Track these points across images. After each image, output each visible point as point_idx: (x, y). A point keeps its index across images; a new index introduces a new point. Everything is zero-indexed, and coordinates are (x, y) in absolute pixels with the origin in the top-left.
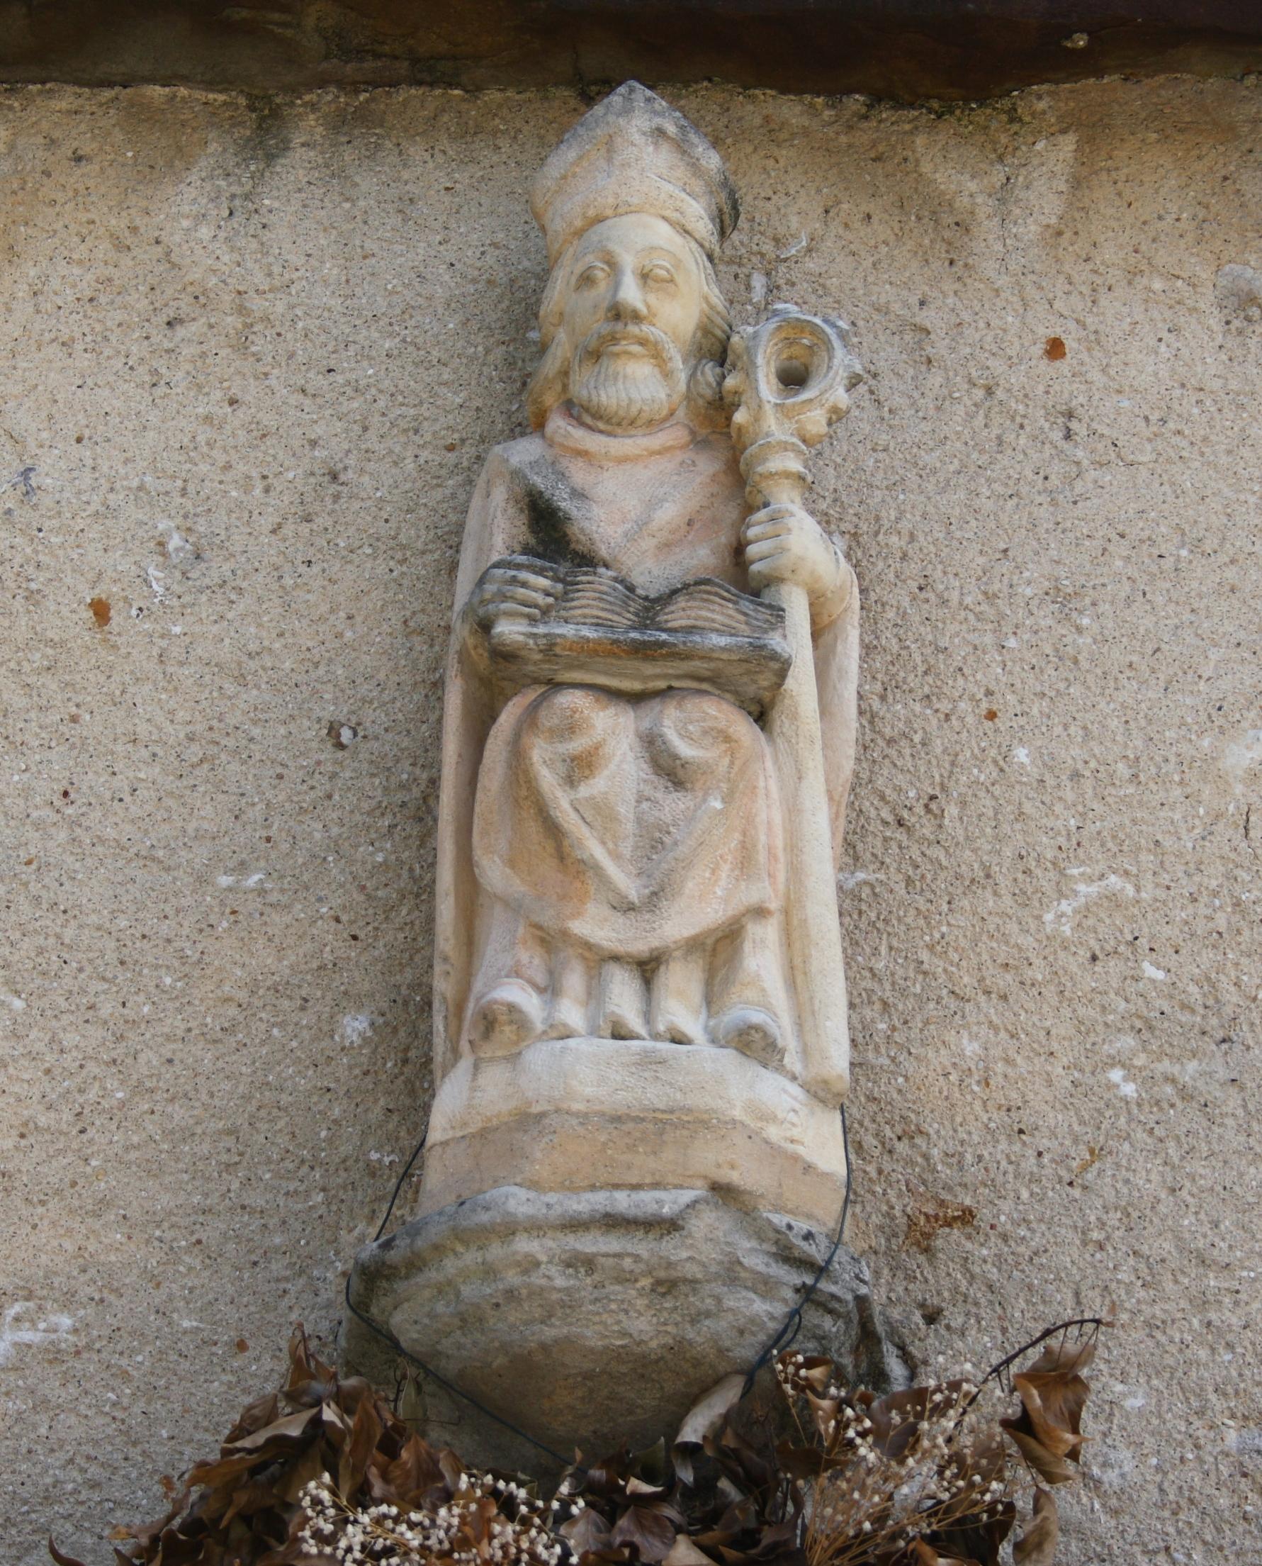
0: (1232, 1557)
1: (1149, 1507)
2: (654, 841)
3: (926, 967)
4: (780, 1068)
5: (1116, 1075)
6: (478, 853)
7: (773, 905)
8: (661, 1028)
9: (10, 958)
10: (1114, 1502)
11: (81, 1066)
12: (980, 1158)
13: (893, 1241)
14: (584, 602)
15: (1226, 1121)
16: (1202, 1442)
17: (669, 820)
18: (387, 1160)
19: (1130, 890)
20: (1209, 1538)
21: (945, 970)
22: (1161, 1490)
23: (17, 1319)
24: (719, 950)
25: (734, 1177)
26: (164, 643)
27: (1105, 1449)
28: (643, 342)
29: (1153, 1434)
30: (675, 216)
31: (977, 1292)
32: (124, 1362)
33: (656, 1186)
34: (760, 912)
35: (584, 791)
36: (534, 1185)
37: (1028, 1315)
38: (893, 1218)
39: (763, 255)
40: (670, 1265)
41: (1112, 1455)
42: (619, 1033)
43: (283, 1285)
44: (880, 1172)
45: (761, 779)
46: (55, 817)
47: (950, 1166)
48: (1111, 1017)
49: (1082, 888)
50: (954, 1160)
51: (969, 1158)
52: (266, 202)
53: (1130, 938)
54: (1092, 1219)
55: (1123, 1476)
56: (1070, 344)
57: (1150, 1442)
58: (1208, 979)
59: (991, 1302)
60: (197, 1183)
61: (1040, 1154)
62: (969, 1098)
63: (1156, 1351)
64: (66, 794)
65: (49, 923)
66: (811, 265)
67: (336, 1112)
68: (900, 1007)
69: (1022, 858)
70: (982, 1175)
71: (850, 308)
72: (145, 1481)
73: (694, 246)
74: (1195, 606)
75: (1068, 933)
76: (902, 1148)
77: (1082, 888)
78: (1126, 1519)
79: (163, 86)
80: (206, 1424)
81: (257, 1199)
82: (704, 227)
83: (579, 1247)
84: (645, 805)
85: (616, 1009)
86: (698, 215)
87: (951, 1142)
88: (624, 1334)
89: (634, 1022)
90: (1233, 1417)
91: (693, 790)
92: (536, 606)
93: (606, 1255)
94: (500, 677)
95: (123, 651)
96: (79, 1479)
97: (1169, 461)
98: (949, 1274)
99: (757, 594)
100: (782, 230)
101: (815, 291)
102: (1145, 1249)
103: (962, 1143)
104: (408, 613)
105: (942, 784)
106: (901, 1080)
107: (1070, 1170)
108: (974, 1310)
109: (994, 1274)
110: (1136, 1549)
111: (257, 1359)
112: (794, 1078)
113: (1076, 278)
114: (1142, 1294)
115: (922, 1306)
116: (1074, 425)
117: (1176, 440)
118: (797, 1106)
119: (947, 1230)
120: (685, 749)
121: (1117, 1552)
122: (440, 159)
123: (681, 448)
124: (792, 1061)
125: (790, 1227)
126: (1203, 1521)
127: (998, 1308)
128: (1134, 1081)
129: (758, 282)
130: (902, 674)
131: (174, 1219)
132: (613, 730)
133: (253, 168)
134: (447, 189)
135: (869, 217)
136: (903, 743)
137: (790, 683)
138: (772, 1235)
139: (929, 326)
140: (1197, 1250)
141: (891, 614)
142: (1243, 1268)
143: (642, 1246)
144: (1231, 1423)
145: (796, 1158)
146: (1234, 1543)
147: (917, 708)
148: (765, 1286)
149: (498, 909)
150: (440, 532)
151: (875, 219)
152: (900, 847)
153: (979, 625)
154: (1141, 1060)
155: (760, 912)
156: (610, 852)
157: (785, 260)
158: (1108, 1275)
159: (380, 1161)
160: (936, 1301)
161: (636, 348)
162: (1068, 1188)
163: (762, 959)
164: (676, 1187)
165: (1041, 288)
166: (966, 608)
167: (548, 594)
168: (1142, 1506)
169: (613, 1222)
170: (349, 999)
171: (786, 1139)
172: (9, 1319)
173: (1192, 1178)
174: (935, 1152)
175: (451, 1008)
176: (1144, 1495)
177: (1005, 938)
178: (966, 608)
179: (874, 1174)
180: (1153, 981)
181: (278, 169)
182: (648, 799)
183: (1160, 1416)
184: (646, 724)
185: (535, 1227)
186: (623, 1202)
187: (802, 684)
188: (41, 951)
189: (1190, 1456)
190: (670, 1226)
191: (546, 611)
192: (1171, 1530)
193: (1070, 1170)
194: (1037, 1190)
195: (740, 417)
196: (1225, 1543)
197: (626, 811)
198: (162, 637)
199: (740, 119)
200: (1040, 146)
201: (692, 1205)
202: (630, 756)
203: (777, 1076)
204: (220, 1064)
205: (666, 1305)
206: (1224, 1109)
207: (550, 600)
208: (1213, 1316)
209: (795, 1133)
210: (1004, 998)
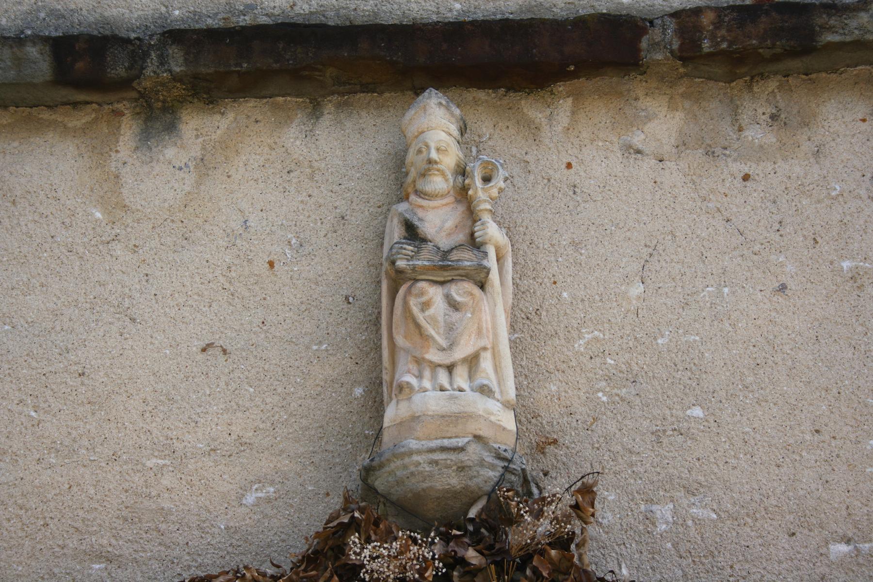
2: (450, 328)
4: (494, 398)
7: (489, 346)
8: (455, 387)
19: (602, 336)
23: (256, 490)
25: (481, 433)
28: (438, 170)
33: (456, 437)
34: (485, 349)
35: (427, 313)
36: (418, 439)
42: (442, 389)
49: (586, 336)
66: (490, 143)
72: (299, 539)
77: (586, 336)
78: (611, 535)
82: (456, 133)
86: (454, 129)
88: (449, 484)
89: (447, 386)
99: (479, 248)
109: (565, 459)
115: (542, 470)
116: (576, 190)
122: (371, 116)
129: (474, 149)
132: (435, 294)
137: (490, 276)
143: (453, 456)
149: (402, 352)
155: (485, 349)
161: (436, 172)
169: (443, 449)
170: (356, 383)
185: (419, 452)
187: (494, 276)
190: (462, 449)
195: (470, 192)
197: (441, 319)
201: (468, 442)
208: (635, 469)
209: (499, 418)
210: (563, 372)
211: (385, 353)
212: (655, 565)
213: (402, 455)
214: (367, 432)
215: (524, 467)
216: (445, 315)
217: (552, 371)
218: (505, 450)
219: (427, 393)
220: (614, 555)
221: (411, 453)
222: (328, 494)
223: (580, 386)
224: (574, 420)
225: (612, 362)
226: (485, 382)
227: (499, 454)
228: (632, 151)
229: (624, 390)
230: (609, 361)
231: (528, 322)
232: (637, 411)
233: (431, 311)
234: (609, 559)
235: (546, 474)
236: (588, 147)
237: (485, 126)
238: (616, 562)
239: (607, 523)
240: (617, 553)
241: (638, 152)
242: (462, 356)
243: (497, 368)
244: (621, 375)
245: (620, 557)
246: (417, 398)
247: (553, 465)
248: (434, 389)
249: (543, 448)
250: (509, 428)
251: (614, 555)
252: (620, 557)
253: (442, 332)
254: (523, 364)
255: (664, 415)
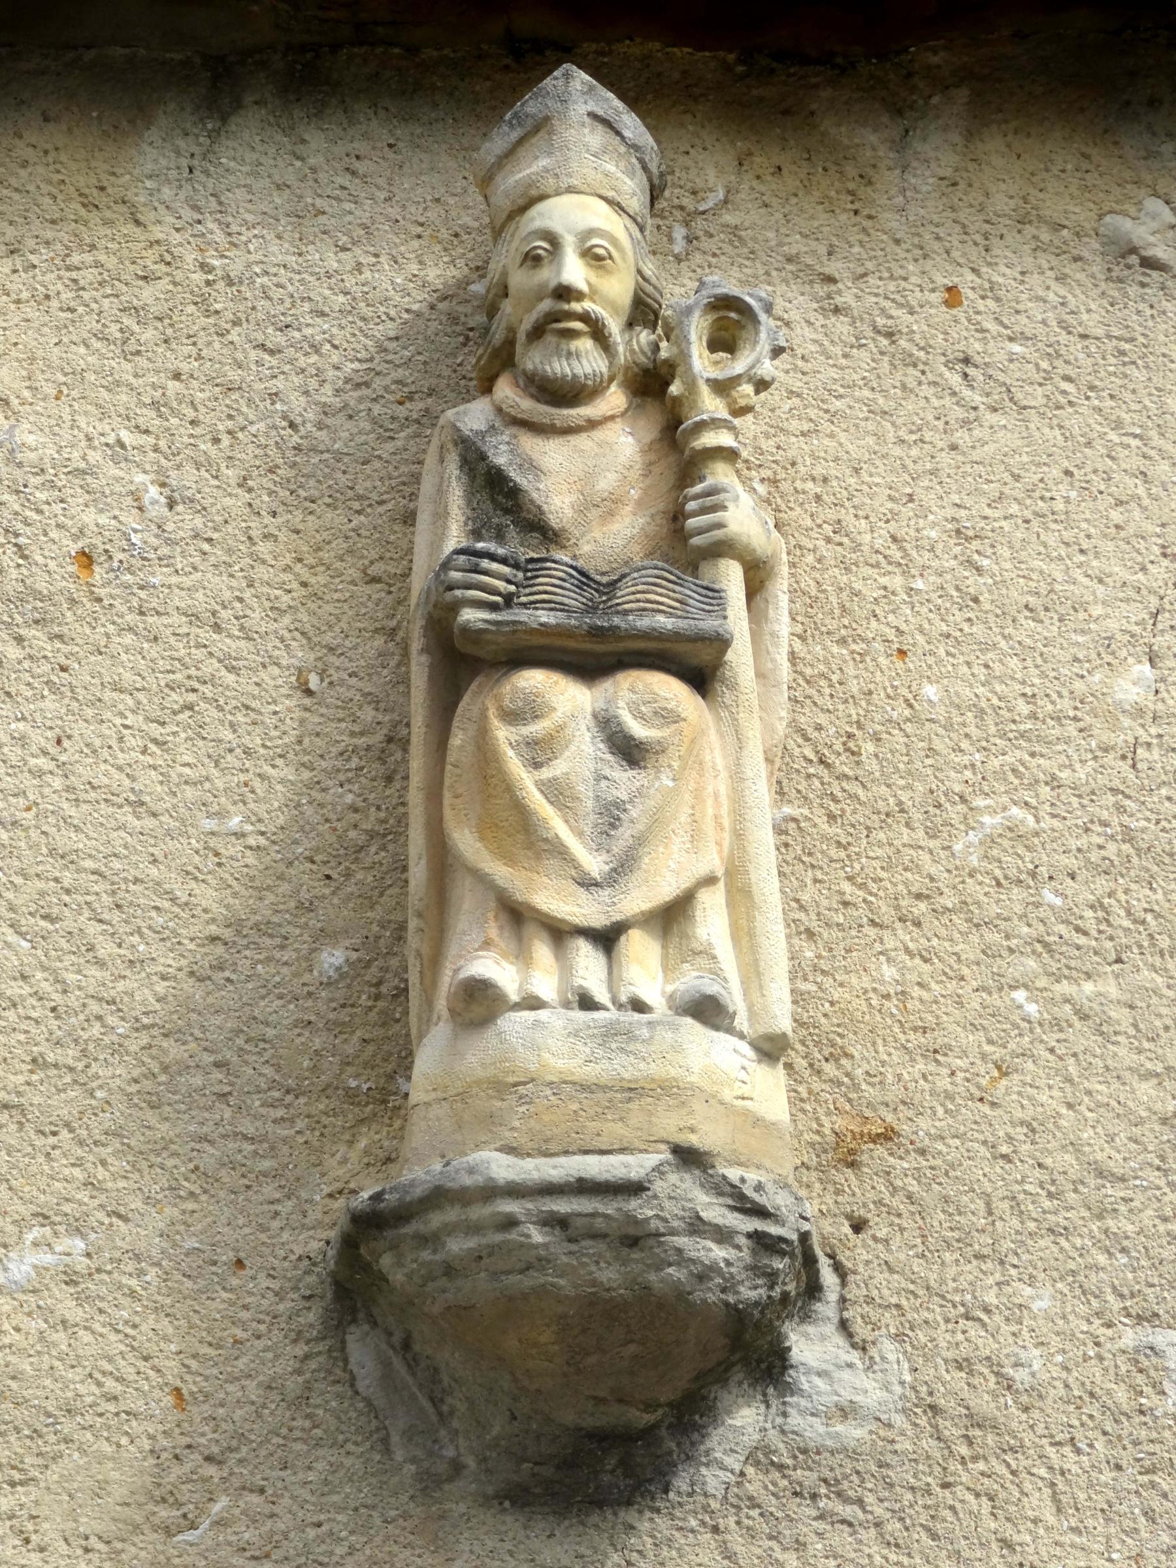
0: (1129, 1446)
1: (1055, 1402)
2: (611, 815)
3: (848, 898)
4: (730, 1030)
5: (1020, 995)
6: (448, 813)
7: (720, 873)
8: (623, 999)
9: (15, 902)
10: (1024, 1399)
11: (84, 1005)
12: (899, 1077)
13: (823, 1156)
14: (541, 588)
15: (1119, 1038)
16: (1102, 1339)
17: (625, 797)
18: (365, 1087)
19: (1031, 820)
20: (1108, 1429)
21: (864, 900)
22: (1067, 1386)
23: (35, 1244)
24: (671, 917)
25: (694, 1140)
26: (143, 594)
27: (1017, 1350)
28: (585, 318)
29: (1058, 1334)
30: (610, 194)
31: (897, 1202)
32: (133, 1282)
33: (622, 1150)
34: (710, 881)
35: (546, 773)
36: (510, 1150)
37: (945, 1225)
38: (823, 1136)
39: (682, 208)
40: (636, 1222)
41: (1023, 1355)
42: (587, 1003)
43: (273, 1208)
44: (810, 1092)
45: (708, 751)
46: (51, 766)
47: (872, 1085)
48: (1015, 941)
49: (987, 819)
50: (877, 1080)
51: (890, 1078)
52: (223, 160)
53: (1031, 866)
54: (1001, 1134)
55: (1033, 1375)
56: (966, 292)
57: (1055, 1342)
58: (1101, 905)
59: (913, 1214)
60: (193, 1113)
61: (953, 1073)
62: (889, 1022)
63: (1060, 1256)
64: (59, 742)
65: (49, 867)
66: (729, 218)
67: (317, 1043)
68: (825, 935)
69: (932, 792)
70: (902, 1094)
71: (765, 258)
72: (157, 1393)
73: (628, 222)
74: (1084, 547)
75: (976, 863)
76: (829, 1069)
77: (987, 819)
78: (1036, 1414)
79: (123, 47)
80: (210, 1339)
81: (248, 1127)
82: (637, 202)
83: (555, 1208)
84: (604, 783)
85: (581, 982)
86: (632, 189)
87: (873, 1063)
88: (594, 1282)
89: (601, 995)
90: (1128, 1315)
91: (645, 768)
92: (499, 594)
93: (580, 1215)
94: (464, 662)
95: (106, 602)
96: (97, 1392)
97: (1059, 407)
98: (873, 1188)
99: (693, 567)
100: (700, 183)
101: (731, 242)
102: (1048, 1161)
103: (883, 1063)
104: (366, 562)
105: (858, 722)
106: (827, 1005)
107: (979, 1087)
108: (897, 1221)
109: (913, 1186)
110: (1044, 1440)
111: (253, 1278)
112: (742, 1036)
113: (972, 229)
114: (1047, 1204)
115: (849, 1217)
116: (971, 371)
117: (1065, 386)
118: (746, 1063)
119: (871, 1146)
120: (638, 730)
121: (1028, 1444)
122: (382, 113)
123: (623, 414)
124: (741, 1022)
125: (743, 1180)
126: (1104, 1413)
127: (918, 1217)
128: (1037, 1002)
129: (679, 233)
130: (820, 616)
131: (173, 1147)
132: (566, 698)
133: (210, 126)
134: (390, 146)
135: (780, 169)
136: (823, 683)
137: (730, 656)
138: (728, 1189)
139: (837, 276)
140: (1096, 1162)
141: (810, 559)
142: (1136, 1178)
143: (609, 1207)
144: (1126, 1321)
145: (746, 1113)
146: (1131, 1434)
147: (835, 649)
148: (723, 1235)
149: (468, 882)
150: (393, 482)
151: (785, 171)
152: (822, 784)
153: (890, 568)
154: (1042, 982)
155: (710, 881)
156: (571, 829)
157: (703, 213)
158: (1017, 1188)
159: (358, 1087)
160: (862, 1212)
161: (578, 325)
162: (979, 1104)
163: (712, 920)
164: (641, 1151)
165: (938, 238)
166: (877, 552)
167: (509, 582)
168: (1049, 1401)
169: (584, 1187)
170: (325, 936)
171: (737, 1098)
172: (28, 1243)
173: (1089, 1093)
174: (859, 1072)
175: (426, 963)
176: (1052, 1392)
177: (917, 868)
178: (877, 552)
179: (805, 1095)
180: (1052, 907)
181: (233, 128)
182: (606, 778)
183: (1064, 1317)
184: (600, 704)
185: (515, 1191)
186: (594, 1167)
187: (740, 657)
188: (42, 894)
189: (1091, 1353)
190: (635, 1188)
191: (509, 599)
192: (1076, 1423)
193: (979, 1087)
194: (950, 1106)
195: (675, 389)
196: (1125, 1433)
197: (585, 792)
198: (142, 588)
199: (659, 75)
200: (935, 100)
201: (658, 1169)
202: (588, 736)
203: (728, 1037)
204: (210, 1000)
205: (634, 1256)
206: (1118, 1028)
207: (512, 588)
208: (1110, 1222)
209: (745, 1090)
210: (918, 924)
211: (418, 873)
212: (1155, 1504)
213: (463, 1197)
214: (353, 1083)
215: (806, 1227)
216: (600, 777)
217: (886, 920)
218: (759, 1187)
219: (542, 1014)
220: (1043, 1472)
221: (492, 1191)
222: (240, 1263)
223: (966, 971)
224: (945, 1071)
225: (1058, 901)
226: (712, 988)
227: (742, 1197)
228: (1134, 259)
229: (1088, 987)
230: (1049, 897)
231: (821, 770)
232: (1122, 1052)
233: (557, 769)
234: (1028, 1487)
235: (858, 1226)
236: (1009, 239)
237: (711, 172)
238: (1047, 1491)
239: (1028, 1379)
240: (1051, 1468)
241: (1149, 263)
242: (646, 906)
243: (744, 933)
244: (1082, 940)
245: (1059, 1480)
246: (513, 1023)
247: (879, 1203)
248: (567, 1005)
249: (852, 1152)
250: (771, 1117)
251: (1043, 1472)
252: (1059, 1480)
253: (588, 830)
254: (805, 897)
255: (762, 182)
